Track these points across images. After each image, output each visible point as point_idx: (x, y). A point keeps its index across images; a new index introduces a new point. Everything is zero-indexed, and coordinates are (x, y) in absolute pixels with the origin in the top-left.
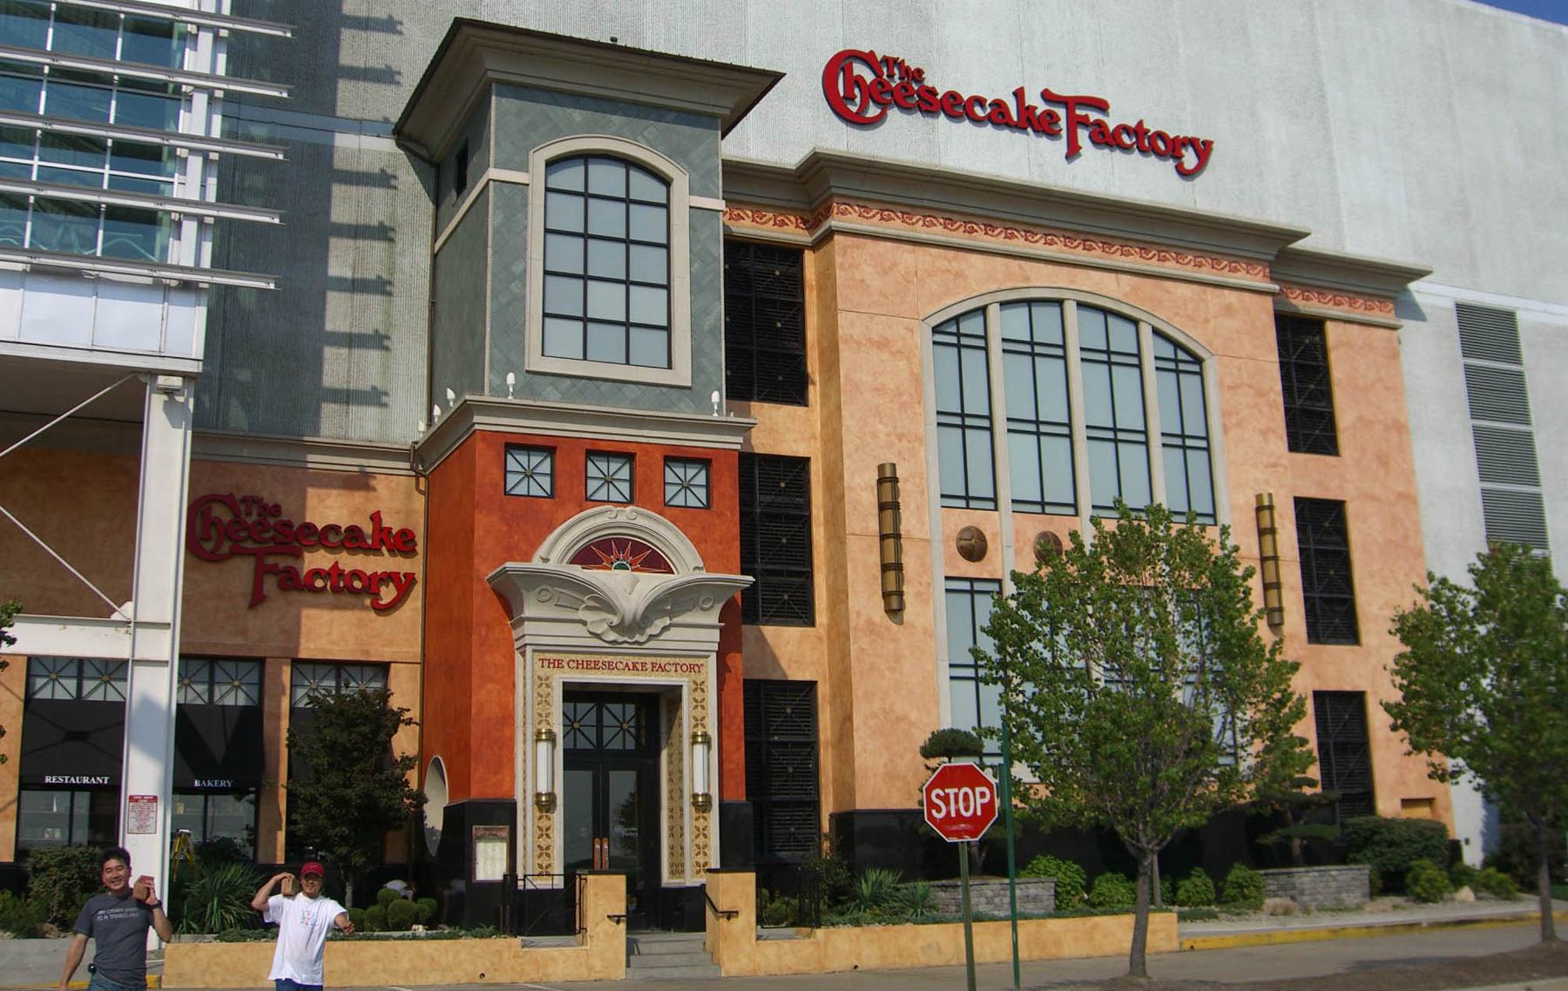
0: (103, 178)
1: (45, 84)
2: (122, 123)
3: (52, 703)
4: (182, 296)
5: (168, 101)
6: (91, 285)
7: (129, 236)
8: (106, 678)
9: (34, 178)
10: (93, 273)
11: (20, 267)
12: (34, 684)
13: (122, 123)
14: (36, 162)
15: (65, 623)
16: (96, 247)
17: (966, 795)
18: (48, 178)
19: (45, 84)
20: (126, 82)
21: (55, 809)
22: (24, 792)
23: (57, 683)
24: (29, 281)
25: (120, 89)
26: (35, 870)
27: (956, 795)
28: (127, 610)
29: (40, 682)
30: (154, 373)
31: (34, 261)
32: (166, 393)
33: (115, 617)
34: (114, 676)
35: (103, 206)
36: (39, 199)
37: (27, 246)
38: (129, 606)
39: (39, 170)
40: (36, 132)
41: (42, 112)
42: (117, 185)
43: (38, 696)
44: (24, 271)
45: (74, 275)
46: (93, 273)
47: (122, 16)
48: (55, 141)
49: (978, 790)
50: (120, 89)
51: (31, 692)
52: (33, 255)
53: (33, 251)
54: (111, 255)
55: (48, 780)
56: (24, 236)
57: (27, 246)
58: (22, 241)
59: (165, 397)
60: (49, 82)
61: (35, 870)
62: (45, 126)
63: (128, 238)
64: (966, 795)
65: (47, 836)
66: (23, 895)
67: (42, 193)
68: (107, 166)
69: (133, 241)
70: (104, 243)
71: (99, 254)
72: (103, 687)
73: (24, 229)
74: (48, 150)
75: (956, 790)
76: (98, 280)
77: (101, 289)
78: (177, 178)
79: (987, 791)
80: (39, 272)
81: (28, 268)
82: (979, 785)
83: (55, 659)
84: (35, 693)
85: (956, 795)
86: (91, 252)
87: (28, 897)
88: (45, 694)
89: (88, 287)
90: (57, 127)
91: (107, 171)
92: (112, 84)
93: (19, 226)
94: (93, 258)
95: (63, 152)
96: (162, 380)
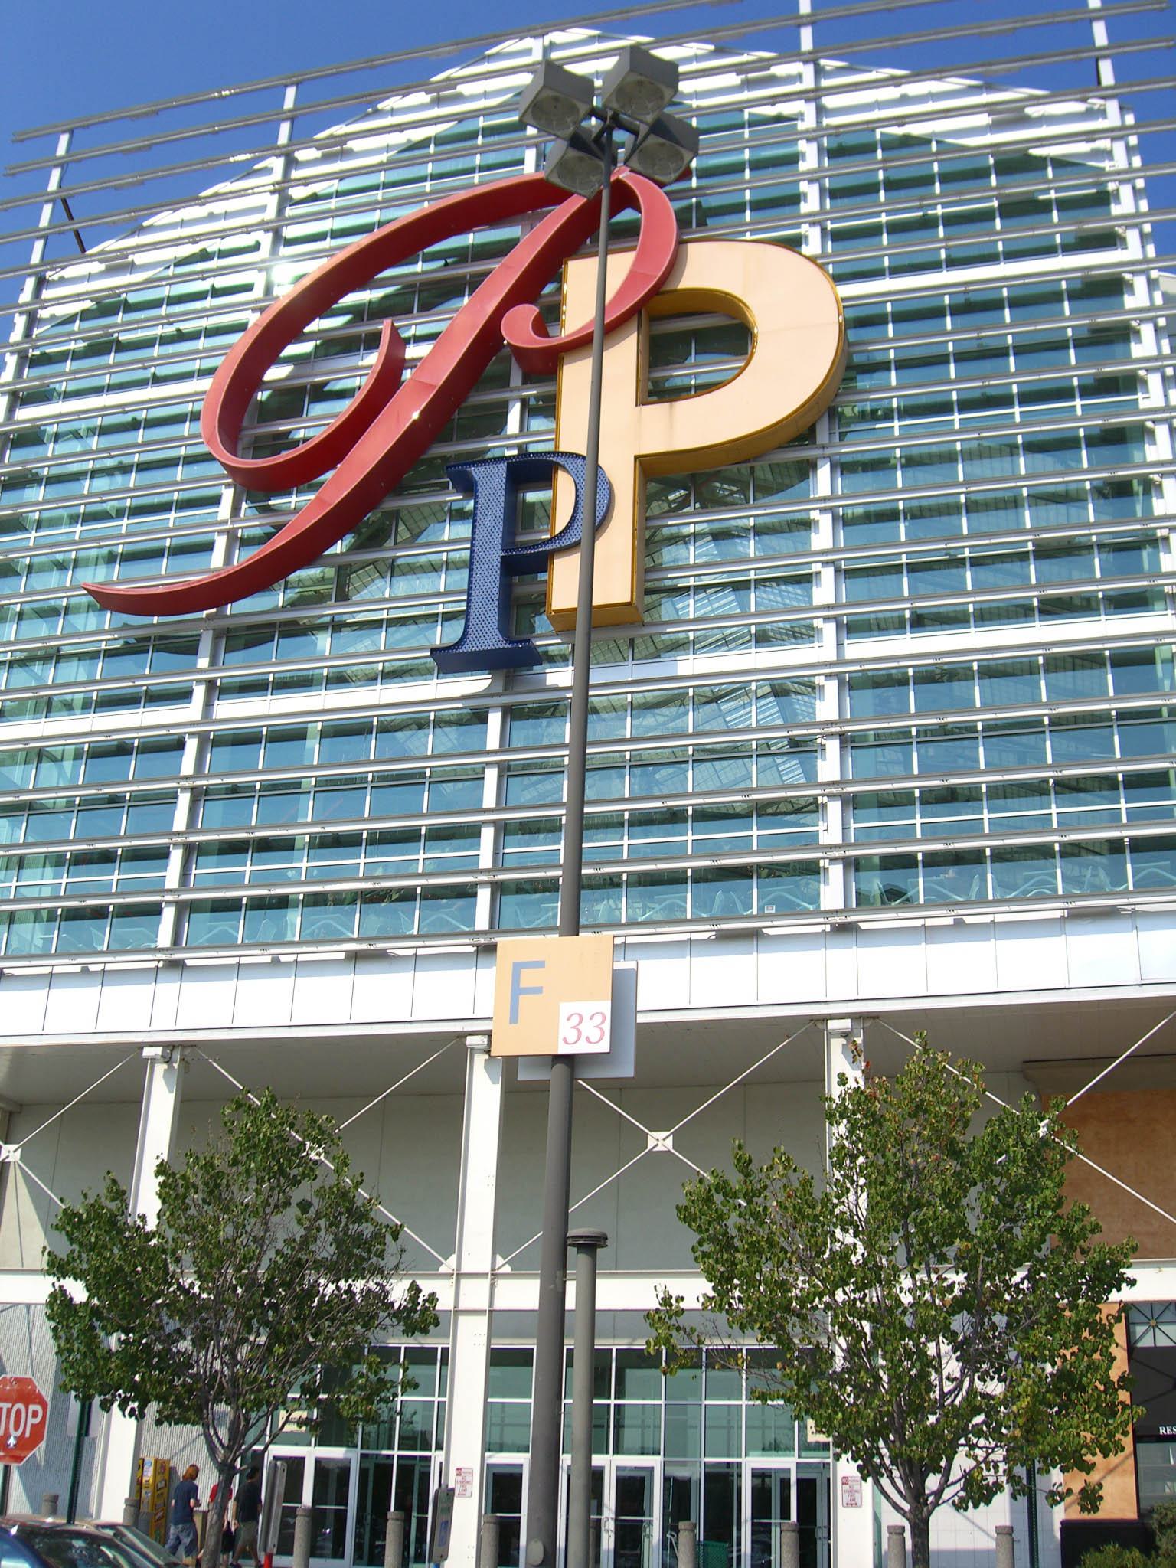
0: (915, 829)
1: (1047, 734)
2: (1129, 754)
3: (1155, 1350)
4: (842, 939)
5: (1165, 726)
6: (1130, 921)
7: (783, 887)
8: (1153, 1323)
9: (1055, 825)
10: (1129, 908)
11: (1058, 914)
12: (1135, 1333)
13: (1129, 754)
14: (1054, 810)
15: (1159, 1265)
16: (1126, 882)
17: (19, 1412)
18: (1000, 827)
19: (914, 744)
20: (1123, 715)
21: (1172, 1462)
22: (1138, 1445)
23: (1157, 1330)
24: (1068, 927)
25: (1052, 728)
26: (1162, 1527)
27: (9, 1411)
28: (449, 1265)
29: (1140, 1330)
30: (825, 1018)
31: (1071, 906)
32: (845, 1037)
33: (443, 1269)
34: (1160, 1320)
35: (1126, 840)
36: (1062, 844)
37: (1060, 892)
38: (453, 1260)
39: (990, 823)
40: (913, 793)
41: (1050, 761)
42: (1135, 816)
43: (1140, 1345)
44: (1063, 917)
45: (1111, 913)
46: (1129, 908)
47: (1107, 653)
48: (1068, 788)
49: (32, 1407)
50: (1052, 728)
51: (1132, 1341)
52: (1069, 900)
53: (1067, 897)
54: (1144, 886)
55: (1162, 1431)
56: (1056, 884)
57: (1060, 892)
58: (1055, 889)
59: (844, 1041)
60: (918, 743)
61: (1162, 1527)
62: (1055, 774)
63: (1155, 867)
64: (19, 1412)
65: (1167, 1490)
66: (1153, 1553)
67: (1065, 839)
68: (1123, 800)
69: (789, 893)
70: (1133, 876)
71: (1131, 888)
72: (1151, 1333)
73: (1055, 878)
74: (1132, 791)
75: (9, 1405)
76: (1135, 914)
77: (1139, 922)
78: (821, 826)
79: (38, 1408)
80: (1077, 916)
81: (1066, 913)
82: (35, 1403)
83: (1151, 1304)
84: (1136, 1342)
85: (9, 1411)
86: (1122, 888)
87: (1158, 1555)
88: (1146, 1342)
89: (1128, 923)
90: (1066, 773)
91: (918, 821)
92: (1112, 720)
93: (231, 927)
94: (1126, 893)
95: (1030, 799)
96: (833, 1025)
